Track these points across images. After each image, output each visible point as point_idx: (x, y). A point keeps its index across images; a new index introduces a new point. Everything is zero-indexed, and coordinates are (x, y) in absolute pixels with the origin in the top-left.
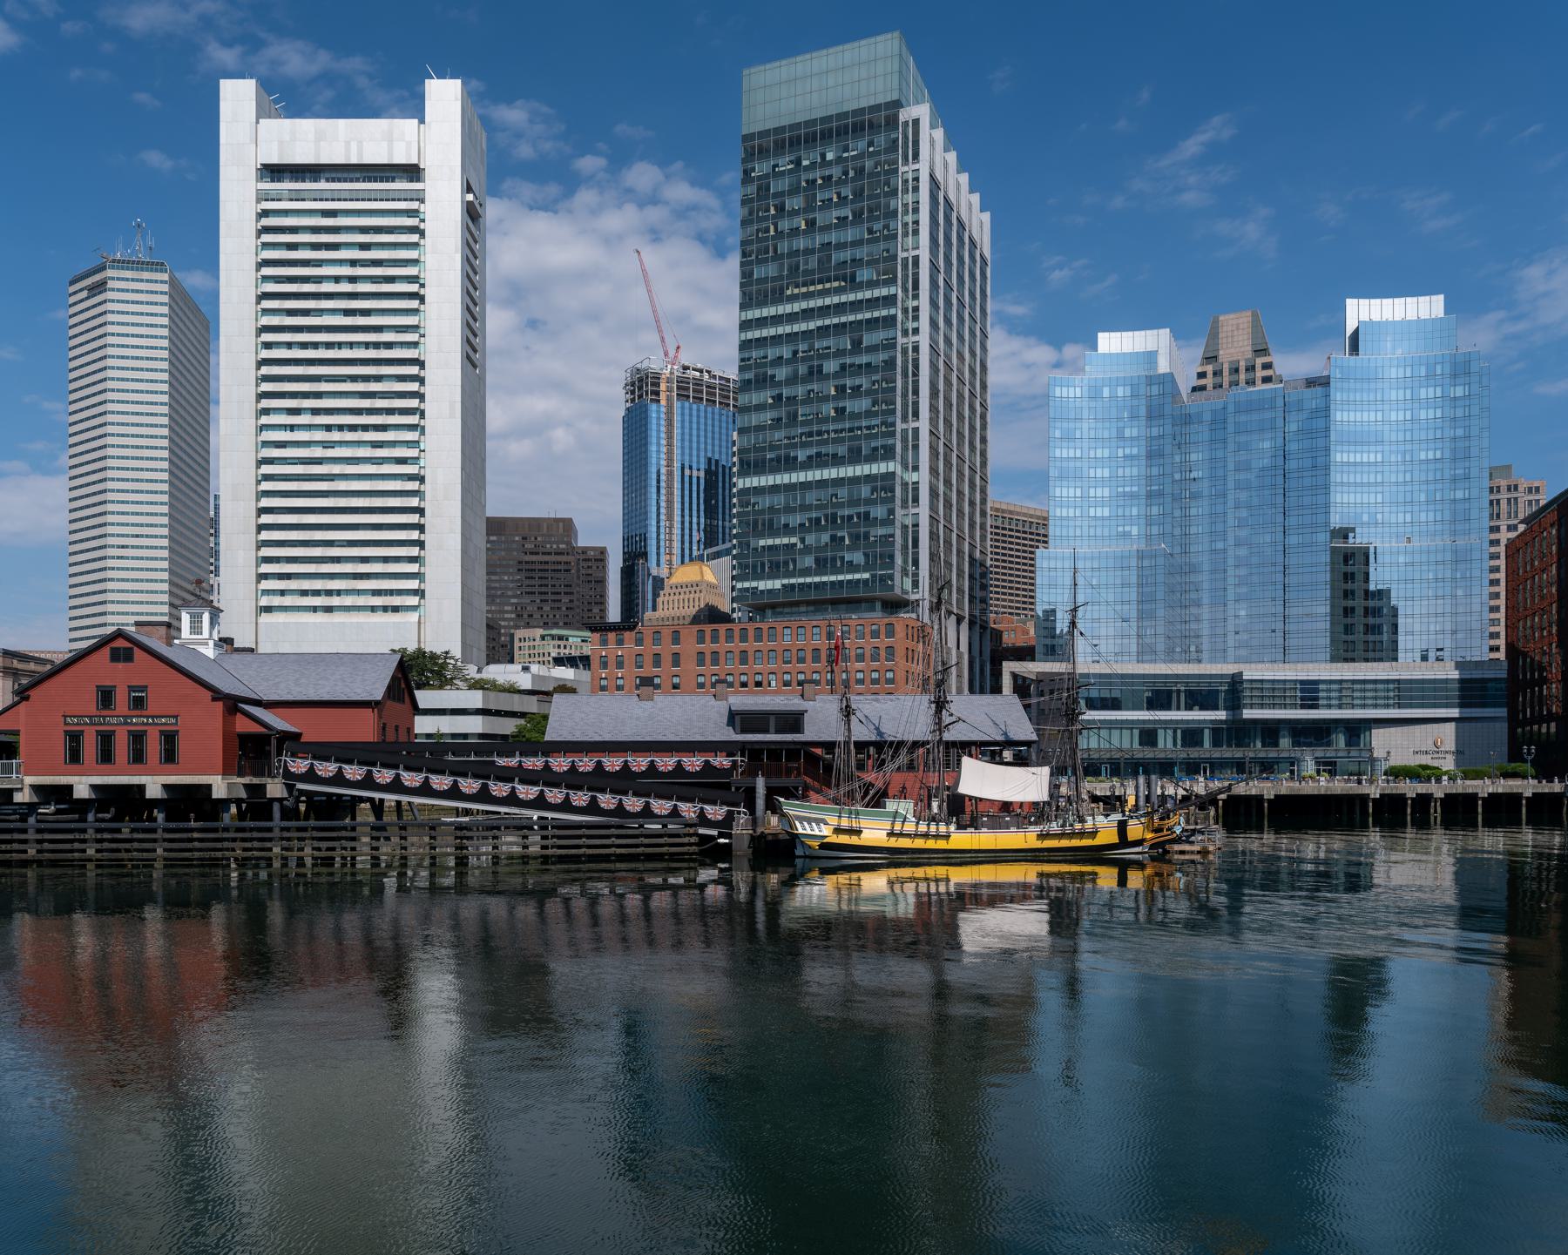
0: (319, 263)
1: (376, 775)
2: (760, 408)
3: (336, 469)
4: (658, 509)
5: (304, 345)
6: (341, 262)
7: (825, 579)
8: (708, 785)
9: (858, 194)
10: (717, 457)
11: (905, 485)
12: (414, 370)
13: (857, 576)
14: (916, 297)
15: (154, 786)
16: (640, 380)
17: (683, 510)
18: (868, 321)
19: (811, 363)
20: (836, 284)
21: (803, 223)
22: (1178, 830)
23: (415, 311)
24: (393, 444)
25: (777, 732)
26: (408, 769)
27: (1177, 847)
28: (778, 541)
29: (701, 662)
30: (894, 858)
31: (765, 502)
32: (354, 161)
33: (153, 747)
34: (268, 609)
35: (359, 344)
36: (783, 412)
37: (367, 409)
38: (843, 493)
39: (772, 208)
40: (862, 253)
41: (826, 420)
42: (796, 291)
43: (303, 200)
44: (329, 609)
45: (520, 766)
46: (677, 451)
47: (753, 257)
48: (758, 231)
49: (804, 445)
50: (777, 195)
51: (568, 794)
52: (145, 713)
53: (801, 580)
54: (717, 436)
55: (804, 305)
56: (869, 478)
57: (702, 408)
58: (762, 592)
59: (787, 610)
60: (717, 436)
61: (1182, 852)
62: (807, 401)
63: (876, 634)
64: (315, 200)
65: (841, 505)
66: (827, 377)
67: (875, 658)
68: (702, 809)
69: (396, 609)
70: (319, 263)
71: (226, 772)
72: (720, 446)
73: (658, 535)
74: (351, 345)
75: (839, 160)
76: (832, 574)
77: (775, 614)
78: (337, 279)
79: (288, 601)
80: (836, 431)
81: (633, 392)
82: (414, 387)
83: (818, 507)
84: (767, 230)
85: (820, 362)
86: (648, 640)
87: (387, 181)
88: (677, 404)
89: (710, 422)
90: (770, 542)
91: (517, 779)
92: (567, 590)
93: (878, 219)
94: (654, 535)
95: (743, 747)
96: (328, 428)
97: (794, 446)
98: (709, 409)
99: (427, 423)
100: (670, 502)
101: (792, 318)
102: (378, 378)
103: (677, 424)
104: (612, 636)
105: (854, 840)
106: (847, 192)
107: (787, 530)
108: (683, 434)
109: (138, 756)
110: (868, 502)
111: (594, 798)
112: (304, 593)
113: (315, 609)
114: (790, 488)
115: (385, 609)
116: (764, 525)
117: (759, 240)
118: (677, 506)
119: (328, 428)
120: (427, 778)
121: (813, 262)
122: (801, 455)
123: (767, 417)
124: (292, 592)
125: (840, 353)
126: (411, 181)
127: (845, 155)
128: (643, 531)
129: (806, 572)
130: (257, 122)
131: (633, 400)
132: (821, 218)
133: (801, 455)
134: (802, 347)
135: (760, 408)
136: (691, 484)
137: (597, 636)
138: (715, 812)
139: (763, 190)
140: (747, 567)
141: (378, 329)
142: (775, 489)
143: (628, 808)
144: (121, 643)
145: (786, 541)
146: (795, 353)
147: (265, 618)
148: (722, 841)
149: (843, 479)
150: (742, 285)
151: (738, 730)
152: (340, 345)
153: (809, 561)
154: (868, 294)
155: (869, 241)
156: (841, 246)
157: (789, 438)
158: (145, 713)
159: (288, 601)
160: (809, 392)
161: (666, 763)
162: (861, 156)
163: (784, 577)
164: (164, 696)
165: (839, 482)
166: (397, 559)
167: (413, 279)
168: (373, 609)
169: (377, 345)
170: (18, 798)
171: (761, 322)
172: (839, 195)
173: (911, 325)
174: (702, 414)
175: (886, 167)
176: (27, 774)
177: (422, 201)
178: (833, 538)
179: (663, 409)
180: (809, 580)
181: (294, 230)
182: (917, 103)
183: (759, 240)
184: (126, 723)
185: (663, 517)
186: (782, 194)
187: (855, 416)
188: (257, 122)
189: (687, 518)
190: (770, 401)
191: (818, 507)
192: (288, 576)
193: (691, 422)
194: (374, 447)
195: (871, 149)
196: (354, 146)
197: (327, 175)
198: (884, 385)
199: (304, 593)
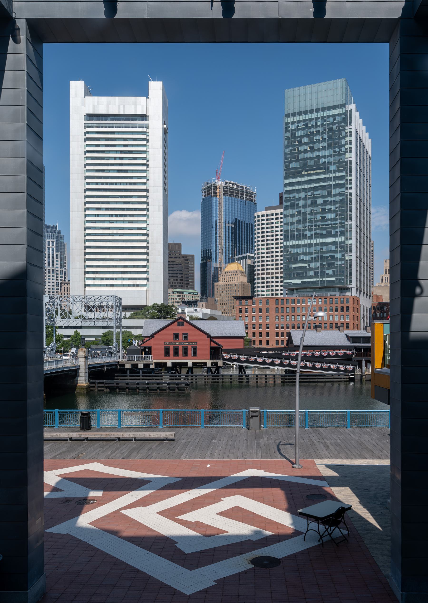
1: (250, 359)
2: (293, 216)
3: (115, 231)
4: (216, 239)
6: (116, 152)
7: (318, 280)
8: (346, 360)
9: (330, 138)
10: (239, 219)
12: (145, 193)
13: (330, 279)
14: (351, 175)
16: (209, 187)
17: (226, 240)
18: (334, 185)
19: (312, 200)
20: (322, 171)
21: (309, 148)
23: (145, 171)
24: (137, 222)
25: (363, 343)
28: (300, 265)
31: (295, 251)
32: (122, 112)
33: (190, 351)
34: (89, 285)
36: (301, 218)
38: (325, 248)
39: (297, 142)
40: (331, 160)
41: (318, 221)
42: (306, 173)
43: (102, 127)
44: (112, 285)
45: (289, 355)
46: (223, 216)
47: (289, 160)
48: (291, 150)
49: (310, 230)
50: (299, 137)
51: (306, 363)
52: (187, 341)
53: (309, 280)
54: (233, 209)
55: (309, 178)
56: (334, 243)
57: (233, 199)
58: (294, 284)
59: (302, 290)
60: (233, 209)
62: (311, 214)
63: (342, 302)
65: (324, 253)
66: (318, 205)
67: (342, 310)
68: (346, 367)
69: (138, 285)
71: (211, 359)
72: (235, 211)
73: (216, 250)
74: (120, 184)
75: (322, 125)
76: (321, 278)
77: (297, 292)
78: (115, 158)
79: (97, 282)
80: (322, 225)
81: (205, 192)
82: (144, 200)
83: (315, 253)
84: (295, 150)
85: (316, 200)
86: (257, 303)
87: (134, 120)
88: (223, 197)
89: (230, 204)
90: (297, 265)
91: (291, 359)
92: (180, 272)
93: (337, 147)
94: (214, 250)
95: (355, 348)
96: (112, 215)
97: (306, 230)
98: (236, 199)
99: (149, 213)
100: (221, 237)
101: (305, 183)
102: (131, 196)
103: (223, 205)
106: (325, 137)
107: (303, 261)
108: (226, 209)
109: (185, 353)
110: (335, 252)
113: (107, 285)
114: (304, 246)
115: (134, 285)
116: (294, 259)
118: (223, 238)
119: (112, 215)
120: (264, 359)
121: (313, 162)
122: (309, 234)
123: (295, 219)
125: (323, 196)
126: (143, 120)
127: (325, 123)
128: (210, 248)
129: (311, 277)
130: (85, 97)
131: (205, 196)
132: (315, 146)
133: (309, 234)
134: (309, 193)
135: (293, 216)
136: (229, 229)
137: (238, 301)
138: (350, 368)
139: (293, 135)
140: (288, 274)
142: (298, 246)
143: (324, 367)
144: (181, 321)
145: (303, 265)
146: (306, 196)
147: (88, 288)
149: (325, 243)
150: (285, 170)
151: (351, 342)
152: (116, 184)
153: (312, 273)
154: (334, 175)
155: (334, 155)
157: (303, 227)
158: (187, 341)
159: (97, 282)
160: (311, 210)
161: (333, 353)
162: (331, 124)
163: (302, 279)
164: (193, 336)
165: (323, 244)
167: (144, 158)
170: (151, 367)
172: (322, 138)
173: (349, 186)
174: (233, 201)
175: (341, 128)
176: (154, 359)
177: (147, 128)
178: (321, 264)
179: (218, 200)
180: (312, 280)
182: (351, 104)
183: (292, 153)
184: (182, 344)
185: (218, 243)
186: (300, 137)
187: (329, 220)
188: (85, 97)
189: (227, 244)
190: (296, 213)
191: (315, 253)
193: (229, 205)
195: (335, 121)
197: (111, 118)
198: (340, 209)
199: (102, 279)
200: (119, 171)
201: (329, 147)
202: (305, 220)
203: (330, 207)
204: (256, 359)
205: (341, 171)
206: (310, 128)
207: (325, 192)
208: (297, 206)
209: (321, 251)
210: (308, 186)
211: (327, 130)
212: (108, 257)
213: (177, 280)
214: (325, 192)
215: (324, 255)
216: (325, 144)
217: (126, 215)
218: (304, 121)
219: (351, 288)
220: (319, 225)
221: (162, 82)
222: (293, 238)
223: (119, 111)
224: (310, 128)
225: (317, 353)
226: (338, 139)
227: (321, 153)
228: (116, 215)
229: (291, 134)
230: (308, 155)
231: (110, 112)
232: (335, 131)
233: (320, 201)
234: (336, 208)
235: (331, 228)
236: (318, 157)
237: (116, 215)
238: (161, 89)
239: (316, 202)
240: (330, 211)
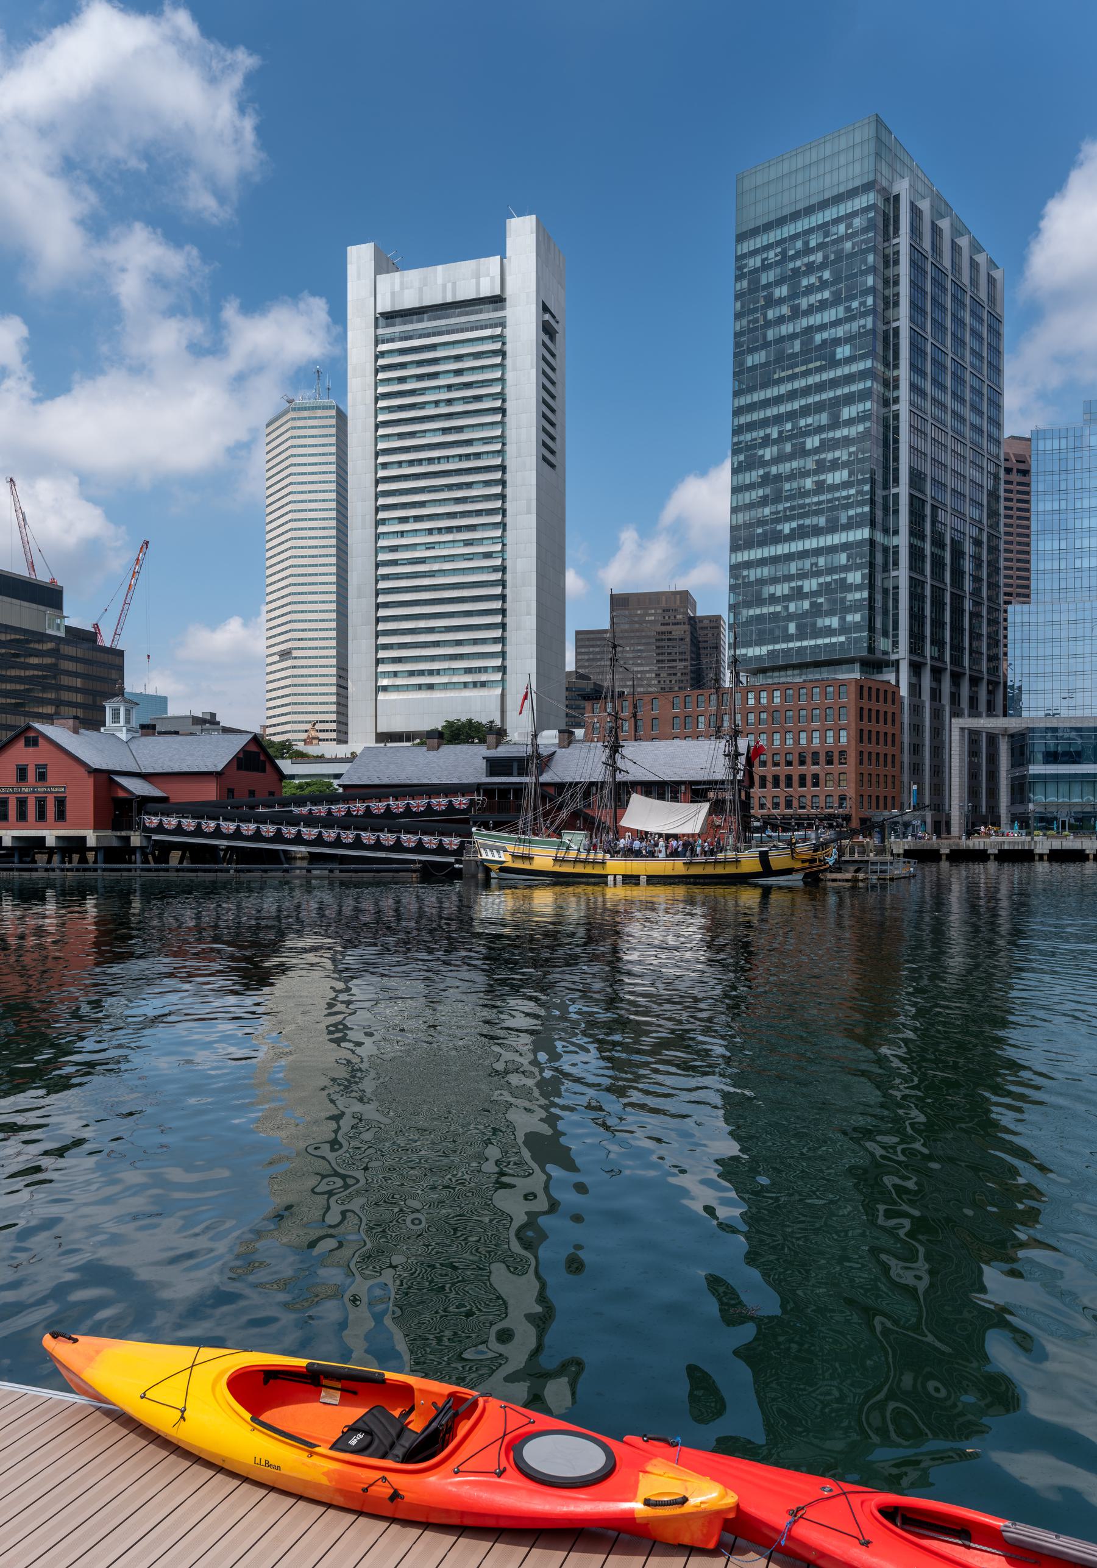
5: (411, 463)
11: (886, 550)
14: (896, 366)
15: (50, 836)
20: (818, 364)
22: (831, 861)
26: (226, 820)
27: (829, 876)
30: (559, 879)
33: (51, 810)
34: (385, 689)
37: (460, 513)
40: (840, 332)
41: (806, 494)
44: (431, 687)
48: (749, 322)
49: (789, 519)
55: (789, 387)
61: (834, 880)
78: (437, 403)
79: (399, 681)
84: (756, 320)
97: (778, 521)
101: (778, 400)
102: (469, 485)
105: (526, 866)
109: (41, 815)
111: (358, 836)
112: (412, 673)
114: (775, 560)
115: (475, 684)
119: (430, 531)
120: (238, 826)
121: (797, 346)
122: (786, 528)
125: (820, 429)
127: (827, 240)
129: (788, 638)
133: (786, 528)
134: (789, 426)
141: (469, 442)
142: (762, 562)
145: (772, 609)
146: (780, 433)
147: (382, 696)
148: (457, 866)
149: (822, 548)
153: (792, 628)
156: (822, 327)
159: (399, 681)
161: (419, 804)
163: (770, 643)
165: (818, 552)
168: (465, 685)
169: (468, 456)
171: (751, 407)
178: (812, 604)
184: (34, 792)
186: (769, 285)
187: (834, 488)
195: (850, 231)
198: (860, 456)
201: (836, 301)
203: (837, 454)
204: (218, 825)
205: (863, 357)
207: (824, 418)
208: (763, 463)
209: (814, 569)
210: (783, 409)
212: (422, 624)
213: (675, 674)
216: (826, 294)
218: (778, 243)
219: (898, 661)
222: (749, 545)
223: (444, 296)
225: (378, 807)
226: (855, 275)
227: (815, 319)
230: (785, 329)
231: (426, 303)
234: (850, 454)
236: (809, 330)
240: (835, 465)
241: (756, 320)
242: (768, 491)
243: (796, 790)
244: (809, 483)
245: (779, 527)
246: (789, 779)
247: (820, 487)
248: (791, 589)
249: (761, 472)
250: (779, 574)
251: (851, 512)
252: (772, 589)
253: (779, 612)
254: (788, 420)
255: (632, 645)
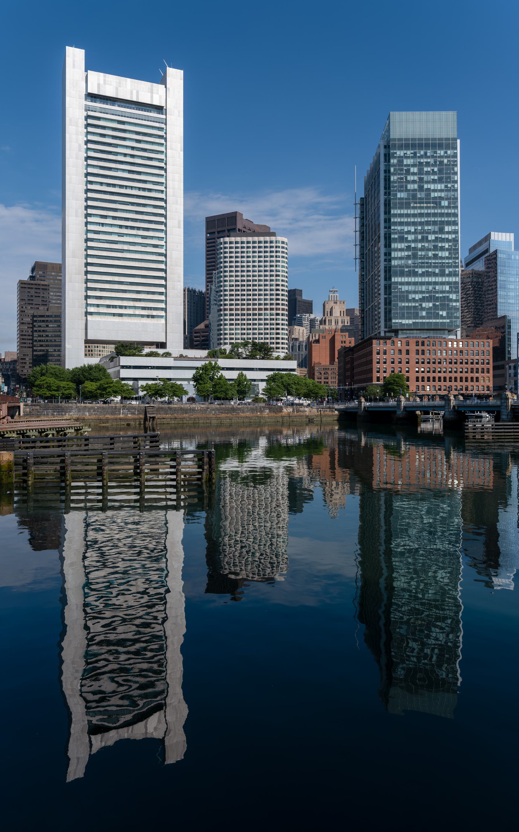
0: (116, 146)
3: (126, 247)
5: (109, 185)
9: (440, 171)
20: (432, 205)
24: (152, 238)
29: (418, 353)
31: (405, 288)
32: (135, 99)
34: (91, 314)
35: (136, 188)
40: (443, 195)
41: (429, 258)
43: (107, 113)
44: (121, 315)
49: (421, 267)
55: (419, 211)
56: (448, 283)
59: (408, 332)
64: (113, 114)
65: (437, 292)
69: (153, 317)
70: (116, 146)
74: (132, 188)
78: (125, 155)
80: (434, 263)
93: (449, 182)
96: (121, 227)
97: (417, 267)
101: (414, 215)
104: (382, 341)
106: (436, 169)
110: (448, 292)
112: (108, 306)
113: (114, 315)
114: (415, 284)
115: (148, 316)
117: (399, 182)
119: (121, 227)
122: (420, 271)
124: (103, 306)
125: (434, 233)
126: (159, 114)
127: (435, 155)
129: (423, 318)
132: (425, 178)
133: (420, 271)
142: (408, 283)
145: (413, 304)
146: (415, 230)
147: (89, 317)
153: (424, 313)
155: (447, 191)
156: (435, 191)
166: (153, 293)
167: (161, 160)
168: (142, 316)
169: (144, 189)
178: (434, 305)
180: (424, 321)
181: (104, 127)
187: (442, 258)
191: (428, 292)
192: (101, 298)
194: (95, 233)
196: (135, 92)
197: (119, 103)
199: (108, 306)
200: (130, 172)
201: (440, 181)
202: (415, 256)
203: (443, 245)
206: (419, 157)
207: (437, 228)
211: (438, 163)
212: (116, 279)
214: (437, 228)
215: (437, 295)
216: (436, 177)
217: (139, 228)
220: (431, 263)
221: (182, 71)
224: (419, 157)
228: (127, 227)
229: (398, 161)
231: (102, 93)
232: (446, 165)
233: (431, 237)
234: (449, 246)
235: (444, 267)
237: (127, 227)
238: (181, 79)
239: (427, 237)
240: (442, 249)
241: (402, 179)
242: (410, 253)
243: (469, 384)
244: (430, 254)
245: (416, 270)
246: (467, 378)
247: (435, 256)
248: (423, 297)
249: (406, 245)
250: (417, 290)
251: (451, 270)
252: (413, 296)
253: (417, 306)
254: (419, 225)
255: (55, 292)
